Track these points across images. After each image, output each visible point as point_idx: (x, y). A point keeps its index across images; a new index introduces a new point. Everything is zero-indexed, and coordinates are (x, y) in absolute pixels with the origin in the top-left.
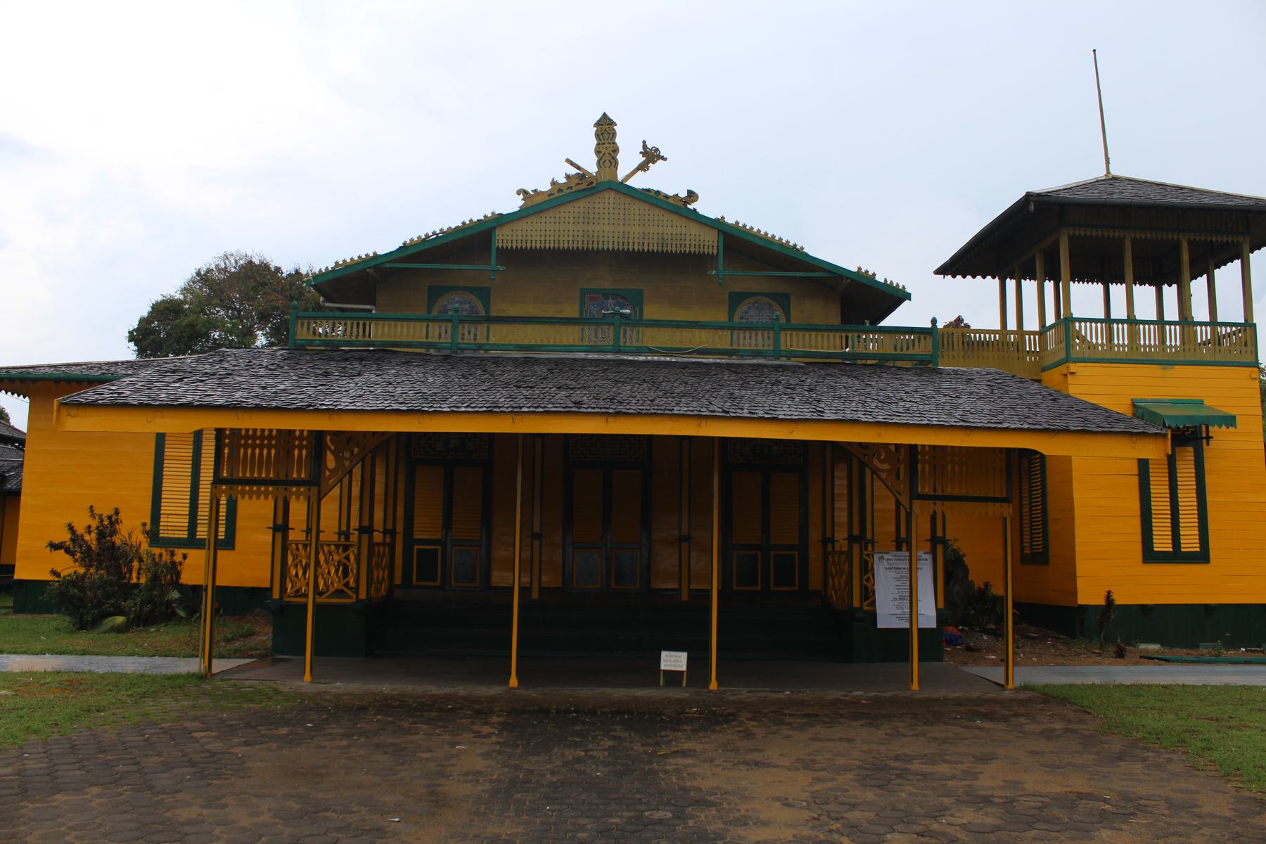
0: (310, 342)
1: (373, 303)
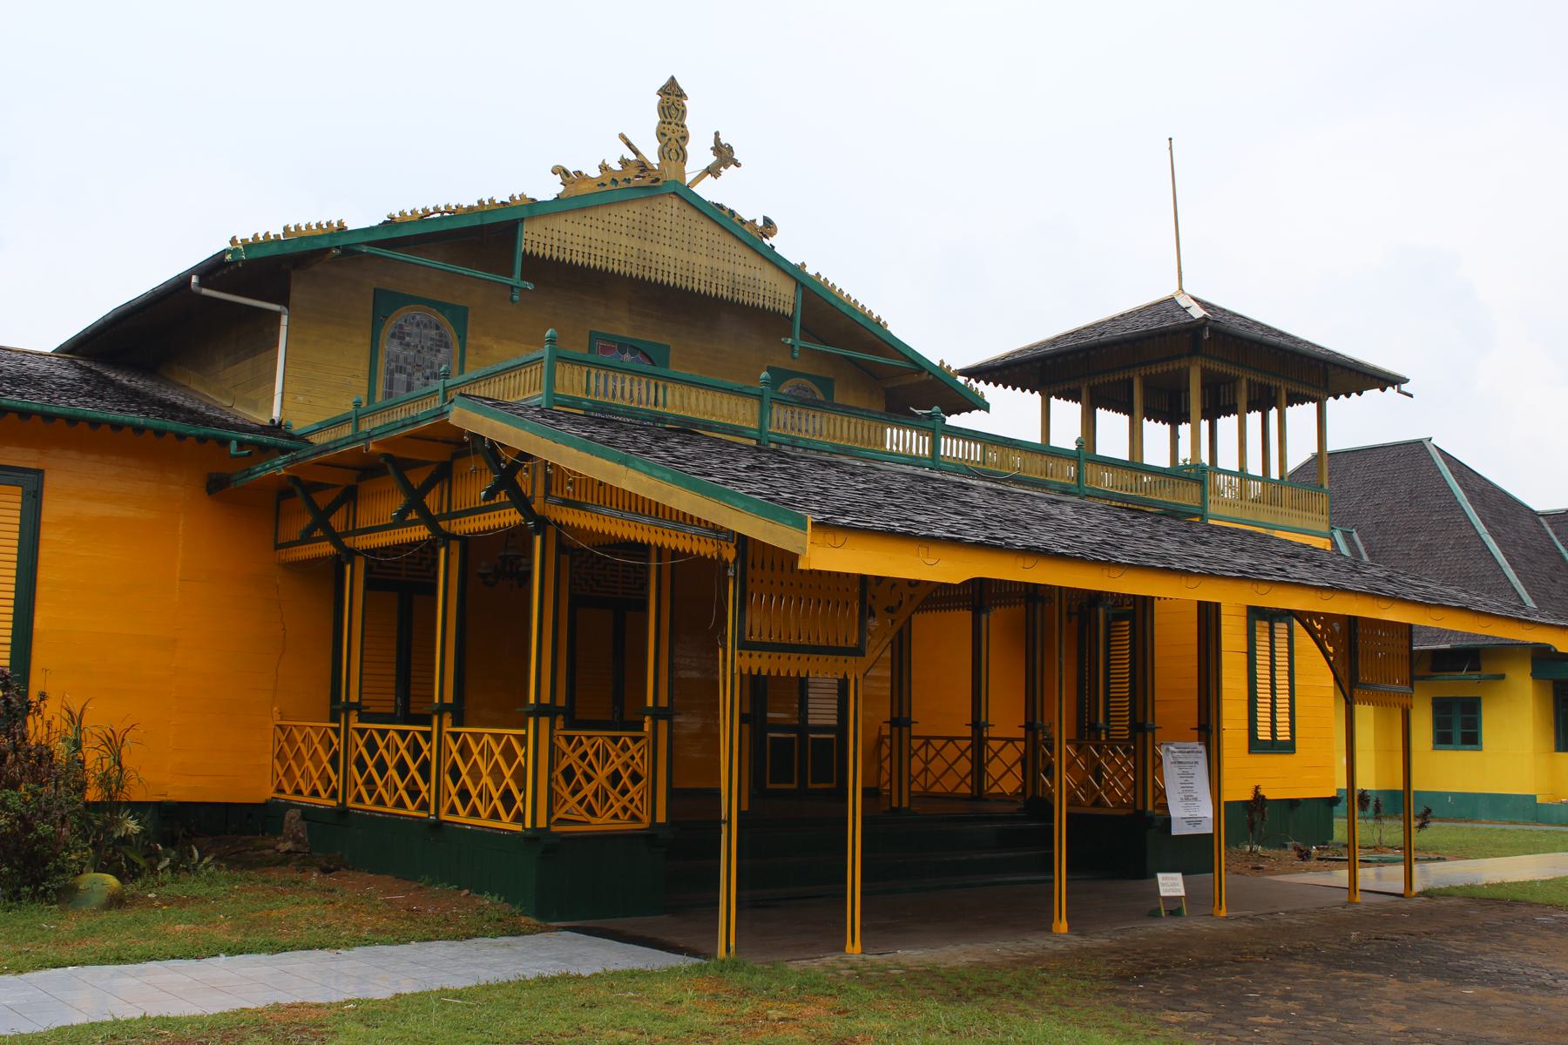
1: (284, 300)
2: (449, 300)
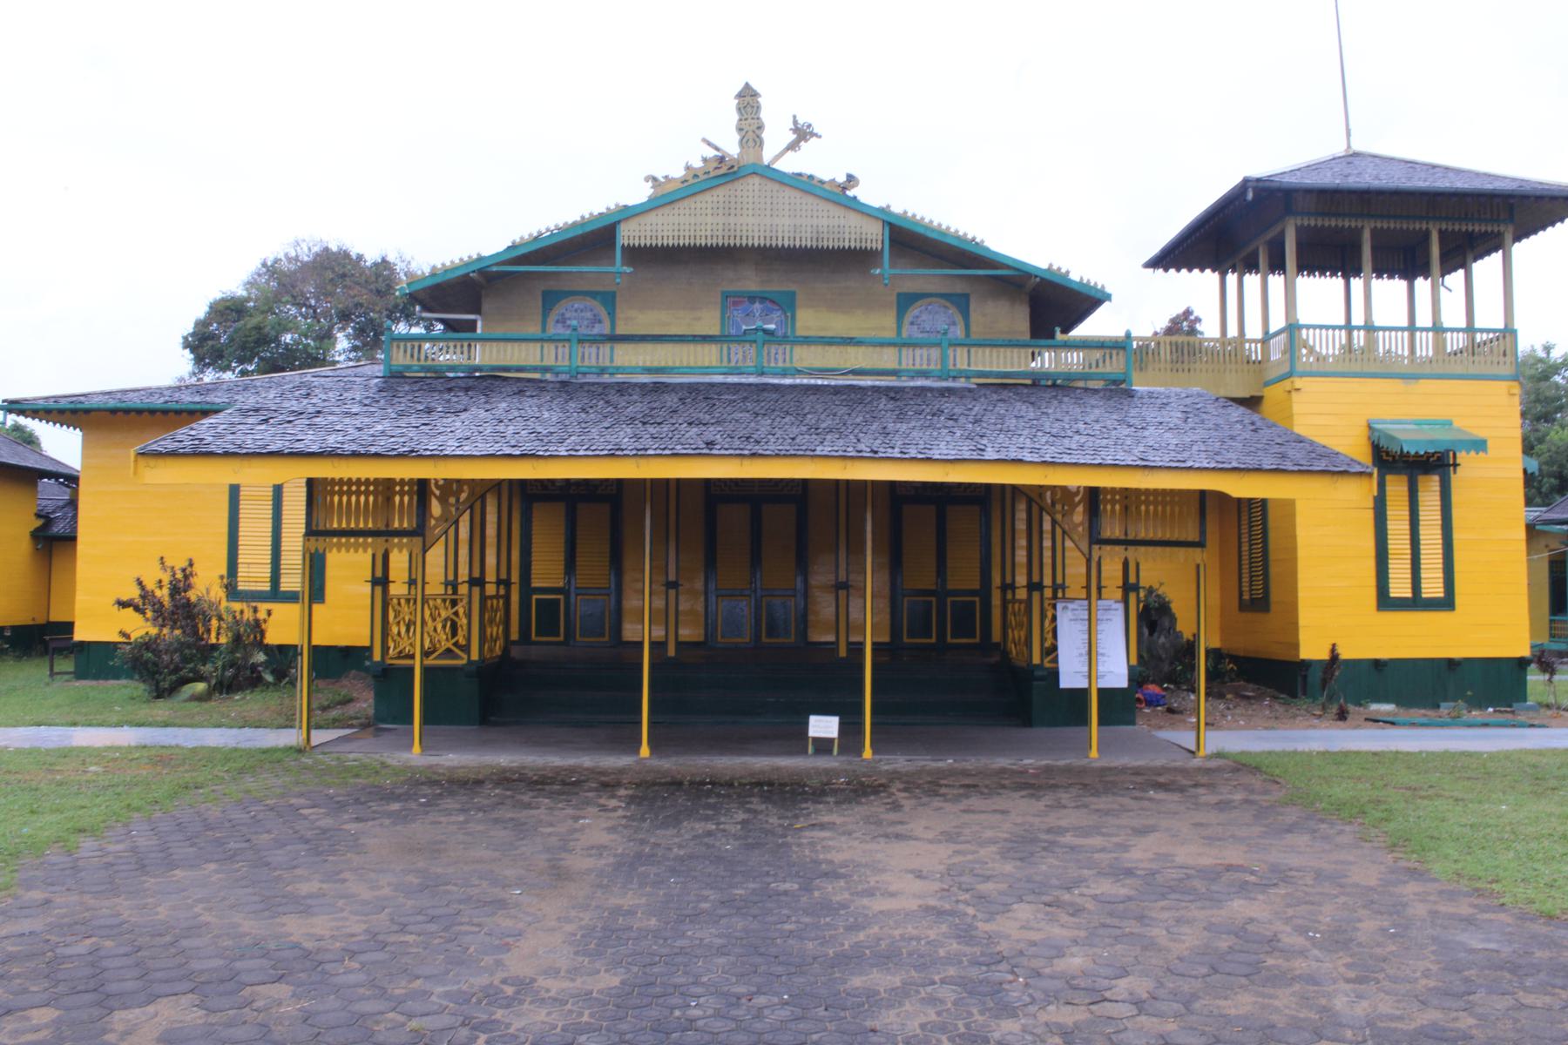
0: (408, 368)
1: (478, 311)
2: (600, 289)
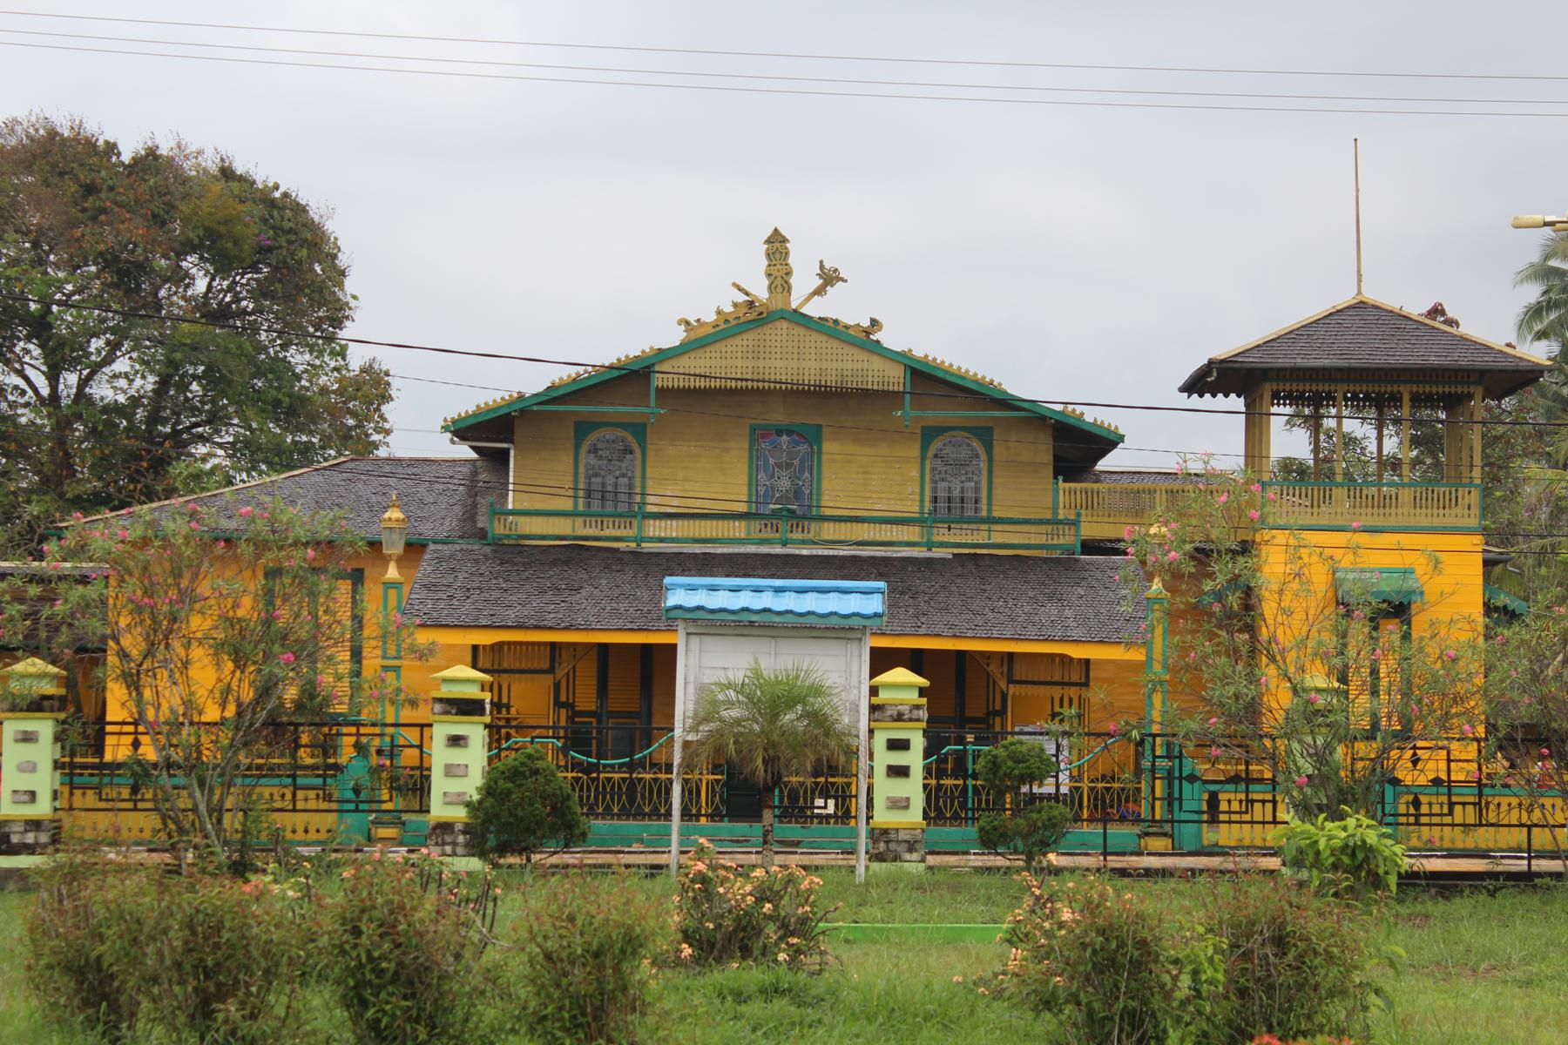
1: (511, 441)
